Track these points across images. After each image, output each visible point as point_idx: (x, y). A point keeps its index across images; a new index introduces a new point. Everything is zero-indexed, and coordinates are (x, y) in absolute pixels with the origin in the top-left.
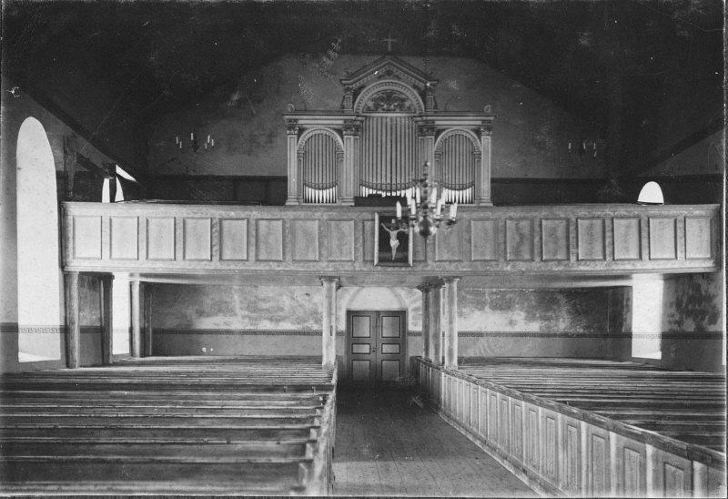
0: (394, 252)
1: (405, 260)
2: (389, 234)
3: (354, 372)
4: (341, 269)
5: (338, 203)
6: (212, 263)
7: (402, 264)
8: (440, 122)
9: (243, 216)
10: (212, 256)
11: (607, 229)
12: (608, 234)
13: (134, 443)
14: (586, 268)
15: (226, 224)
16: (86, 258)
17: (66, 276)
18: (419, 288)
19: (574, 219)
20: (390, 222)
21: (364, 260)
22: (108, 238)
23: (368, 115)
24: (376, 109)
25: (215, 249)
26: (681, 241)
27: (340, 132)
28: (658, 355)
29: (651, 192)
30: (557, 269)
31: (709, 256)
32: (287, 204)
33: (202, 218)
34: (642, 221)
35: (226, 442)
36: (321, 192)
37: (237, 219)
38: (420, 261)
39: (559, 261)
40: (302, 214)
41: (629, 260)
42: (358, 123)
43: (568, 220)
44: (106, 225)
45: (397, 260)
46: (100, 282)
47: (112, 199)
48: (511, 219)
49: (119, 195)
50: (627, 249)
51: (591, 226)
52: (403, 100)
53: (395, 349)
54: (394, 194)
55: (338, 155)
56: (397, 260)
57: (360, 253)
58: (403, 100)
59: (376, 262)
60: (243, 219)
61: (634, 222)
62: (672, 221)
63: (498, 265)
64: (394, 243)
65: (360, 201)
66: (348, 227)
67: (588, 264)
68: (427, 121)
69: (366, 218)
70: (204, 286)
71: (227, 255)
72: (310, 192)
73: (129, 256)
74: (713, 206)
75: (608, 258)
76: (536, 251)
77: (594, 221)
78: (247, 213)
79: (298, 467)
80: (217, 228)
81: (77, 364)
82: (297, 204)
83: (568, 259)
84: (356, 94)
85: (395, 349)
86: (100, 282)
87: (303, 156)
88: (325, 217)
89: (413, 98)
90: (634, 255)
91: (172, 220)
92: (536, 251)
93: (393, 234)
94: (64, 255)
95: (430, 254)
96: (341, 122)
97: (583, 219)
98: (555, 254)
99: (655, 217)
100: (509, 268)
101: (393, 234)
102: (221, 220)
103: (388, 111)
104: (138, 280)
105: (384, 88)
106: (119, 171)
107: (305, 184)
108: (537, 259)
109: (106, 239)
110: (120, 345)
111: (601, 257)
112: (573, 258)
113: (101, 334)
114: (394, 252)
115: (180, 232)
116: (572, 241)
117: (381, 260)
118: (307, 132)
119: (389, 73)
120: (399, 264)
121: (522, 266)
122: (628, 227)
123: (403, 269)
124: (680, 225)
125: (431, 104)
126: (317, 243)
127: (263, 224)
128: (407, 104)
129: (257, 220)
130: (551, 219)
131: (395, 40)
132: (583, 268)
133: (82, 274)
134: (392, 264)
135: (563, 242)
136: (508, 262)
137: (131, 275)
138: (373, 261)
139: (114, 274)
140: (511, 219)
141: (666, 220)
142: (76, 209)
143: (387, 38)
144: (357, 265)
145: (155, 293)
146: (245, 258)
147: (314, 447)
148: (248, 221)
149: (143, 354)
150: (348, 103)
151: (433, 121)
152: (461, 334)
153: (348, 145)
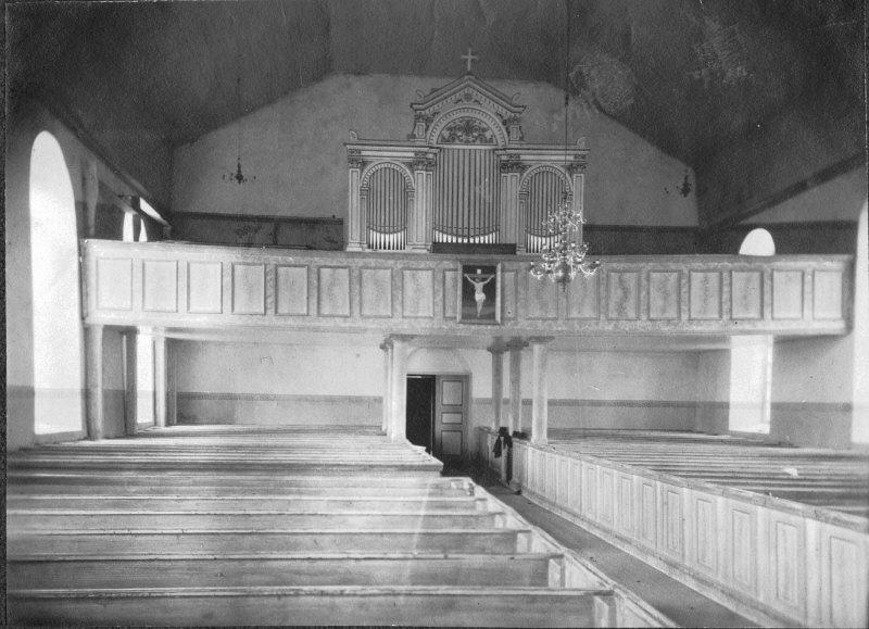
0: (479, 308)
1: (492, 316)
2: (473, 286)
3: (444, 449)
4: (418, 327)
5: (408, 250)
6: (266, 318)
7: (488, 322)
8: (526, 157)
9: (302, 262)
10: (266, 308)
11: (725, 282)
12: (726, 289)
13: (321, 559)
14: (699, 328)
15: (282, 270)
16: (106, 313)
17: (87, 331)
18: (489, 349)
19: (686, 271)
20: (475, 272)
21: (444, 317)
22: (141, 285)
23: (445, 146)
24: (452, 139)
25: (269, 300)
26: (808, 297)
27: (411, 166)
28: (765, 428)
29: (759, 242)
30: (665, 329)
31: (840, 316)
32: (349, 249)
33: (254, 264)
34: (765, 274)
35: (442, 556)
36: (387, 236)
37: (296, 266)
38: (510, 319)
39: (669, 321)
40: (372, 262)
41: (749, 319)
42: (431, 156)
43: (680, 272)
44: (183, 273)
45: (482, 317)
46: (125, 335)
47: (136, 238)
48: (614, 271)
49: (143, 236)
50: (746, 308)
51: (706, 280)
52: (484, 130)
53: (456, 418)
54: (472, 241)
55: (407, 193)
56: (482, 317)
57: (439, 309)
58: (484, 130)
59: (459, 317)
60: (302, 266)
61: (756, 275)
62: (799, 274)
63: (597, 324)
64: (480, 297)
65: (438, 248)
66: (425, 277)
67: (702, 321)
68: (511, 156)
69: (447, 267)
70: (194, 342)
71: (283, 309)
72: (376, 237)
73: (168, 308)
74: (846, 257)
75: (725, 317)
76: (643, 307)
77: (709, 274)
78: (306, 259)
79: (591, 603)
80: (271, 276)
81: (100, 435)
82: (360, 250)
83: (679, 317)
84: (428, 120)
85: (456, 418)
86: (125, 335)
87: (367, 192)
88: (400, 266)
89: (495, 128)
90: (754, 314)
91: (219, 266)
92: (643, 307)
93: (479, 286)
94: (85, 305)
95: (521, 311)
96: (412, 155)
97: (697, 271)
98: (664, 311)
99: (779, 270)
100: (610, 328)
101: (479, 286)
102: (277, 266)
103: (467, 142)
104: (163, 336)
105: (463, 115)
106: (145, 206)
107: (434, 228)
108: (644, 317)
109: (138, 285)
110: (143, 415)
111: (717, 316)
112: (685, 317)
113: (123, 403)
114: (479, 308)
115: (228, 279)
116: (685, 296)
117: (465, 317)
118: (373, 164)
119: (468, 97)
120: (484, 321)
121: (626, 326)
122: (748, 280)
123: (489, 327)
124: (808, 278)
125: (515, 135)
126: (389, 296)
127: (326, 272)
128: (488, 135)
129: (319, 268)
130: (658, 274)
131: (464, 57)
132: (696, 329)
133: (108, 329)
134: (477, 321)
135: (674, 296)
136: (610, 320)
137: (155, 329)
138: (455, 318)
139: (140, 328)
140: (614, 271)
141: (791, 274)
142: (99, 248)
143: (467, 54)
144: (435, 321)
145: (178, 349)
146: (305, 312)
147: (560, 564)
148: (308, 270)
149: (168, 424)
150: (419, 131)
151: (519, 155)
152: (551, 403)
153: (421, 182)
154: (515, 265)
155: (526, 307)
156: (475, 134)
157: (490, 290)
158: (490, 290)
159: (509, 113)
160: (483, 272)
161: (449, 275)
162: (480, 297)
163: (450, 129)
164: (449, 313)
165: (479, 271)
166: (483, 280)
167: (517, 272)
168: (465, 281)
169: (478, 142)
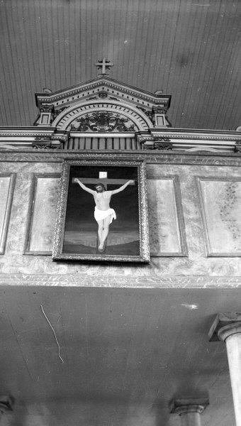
0: (103, 234)
1: (135, 247)
2: (91, 196)
64: (104, 214)
95: (192, 240)
103: (102, 131)
105: (96, 109)
114: (103, 234)
151: (168, 138)
154: (172, 170)
155: (202, 233)
156: (113, 124)
157: (127, 206)
158: (127, 206)
159: (151, 105)
160: (109, 177)
161: (44, 185)
162: (104, 214)
163: (82, 120)
164: (37, 246)
165: (103, 175)
166: (111, 187)
167: (177, 179)
168: (73, 191)
169: (115, 130)
